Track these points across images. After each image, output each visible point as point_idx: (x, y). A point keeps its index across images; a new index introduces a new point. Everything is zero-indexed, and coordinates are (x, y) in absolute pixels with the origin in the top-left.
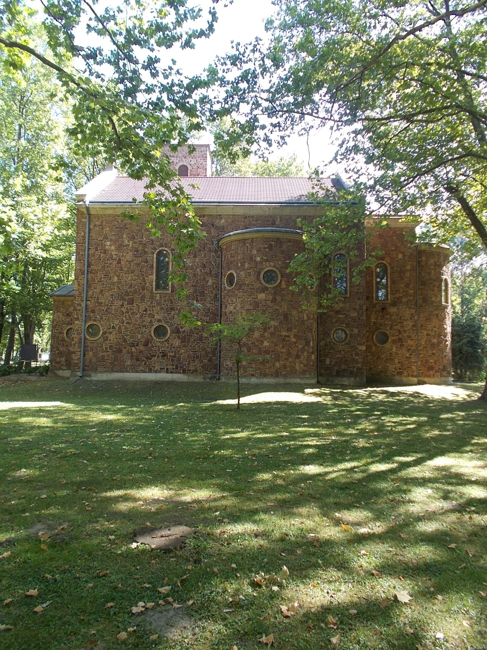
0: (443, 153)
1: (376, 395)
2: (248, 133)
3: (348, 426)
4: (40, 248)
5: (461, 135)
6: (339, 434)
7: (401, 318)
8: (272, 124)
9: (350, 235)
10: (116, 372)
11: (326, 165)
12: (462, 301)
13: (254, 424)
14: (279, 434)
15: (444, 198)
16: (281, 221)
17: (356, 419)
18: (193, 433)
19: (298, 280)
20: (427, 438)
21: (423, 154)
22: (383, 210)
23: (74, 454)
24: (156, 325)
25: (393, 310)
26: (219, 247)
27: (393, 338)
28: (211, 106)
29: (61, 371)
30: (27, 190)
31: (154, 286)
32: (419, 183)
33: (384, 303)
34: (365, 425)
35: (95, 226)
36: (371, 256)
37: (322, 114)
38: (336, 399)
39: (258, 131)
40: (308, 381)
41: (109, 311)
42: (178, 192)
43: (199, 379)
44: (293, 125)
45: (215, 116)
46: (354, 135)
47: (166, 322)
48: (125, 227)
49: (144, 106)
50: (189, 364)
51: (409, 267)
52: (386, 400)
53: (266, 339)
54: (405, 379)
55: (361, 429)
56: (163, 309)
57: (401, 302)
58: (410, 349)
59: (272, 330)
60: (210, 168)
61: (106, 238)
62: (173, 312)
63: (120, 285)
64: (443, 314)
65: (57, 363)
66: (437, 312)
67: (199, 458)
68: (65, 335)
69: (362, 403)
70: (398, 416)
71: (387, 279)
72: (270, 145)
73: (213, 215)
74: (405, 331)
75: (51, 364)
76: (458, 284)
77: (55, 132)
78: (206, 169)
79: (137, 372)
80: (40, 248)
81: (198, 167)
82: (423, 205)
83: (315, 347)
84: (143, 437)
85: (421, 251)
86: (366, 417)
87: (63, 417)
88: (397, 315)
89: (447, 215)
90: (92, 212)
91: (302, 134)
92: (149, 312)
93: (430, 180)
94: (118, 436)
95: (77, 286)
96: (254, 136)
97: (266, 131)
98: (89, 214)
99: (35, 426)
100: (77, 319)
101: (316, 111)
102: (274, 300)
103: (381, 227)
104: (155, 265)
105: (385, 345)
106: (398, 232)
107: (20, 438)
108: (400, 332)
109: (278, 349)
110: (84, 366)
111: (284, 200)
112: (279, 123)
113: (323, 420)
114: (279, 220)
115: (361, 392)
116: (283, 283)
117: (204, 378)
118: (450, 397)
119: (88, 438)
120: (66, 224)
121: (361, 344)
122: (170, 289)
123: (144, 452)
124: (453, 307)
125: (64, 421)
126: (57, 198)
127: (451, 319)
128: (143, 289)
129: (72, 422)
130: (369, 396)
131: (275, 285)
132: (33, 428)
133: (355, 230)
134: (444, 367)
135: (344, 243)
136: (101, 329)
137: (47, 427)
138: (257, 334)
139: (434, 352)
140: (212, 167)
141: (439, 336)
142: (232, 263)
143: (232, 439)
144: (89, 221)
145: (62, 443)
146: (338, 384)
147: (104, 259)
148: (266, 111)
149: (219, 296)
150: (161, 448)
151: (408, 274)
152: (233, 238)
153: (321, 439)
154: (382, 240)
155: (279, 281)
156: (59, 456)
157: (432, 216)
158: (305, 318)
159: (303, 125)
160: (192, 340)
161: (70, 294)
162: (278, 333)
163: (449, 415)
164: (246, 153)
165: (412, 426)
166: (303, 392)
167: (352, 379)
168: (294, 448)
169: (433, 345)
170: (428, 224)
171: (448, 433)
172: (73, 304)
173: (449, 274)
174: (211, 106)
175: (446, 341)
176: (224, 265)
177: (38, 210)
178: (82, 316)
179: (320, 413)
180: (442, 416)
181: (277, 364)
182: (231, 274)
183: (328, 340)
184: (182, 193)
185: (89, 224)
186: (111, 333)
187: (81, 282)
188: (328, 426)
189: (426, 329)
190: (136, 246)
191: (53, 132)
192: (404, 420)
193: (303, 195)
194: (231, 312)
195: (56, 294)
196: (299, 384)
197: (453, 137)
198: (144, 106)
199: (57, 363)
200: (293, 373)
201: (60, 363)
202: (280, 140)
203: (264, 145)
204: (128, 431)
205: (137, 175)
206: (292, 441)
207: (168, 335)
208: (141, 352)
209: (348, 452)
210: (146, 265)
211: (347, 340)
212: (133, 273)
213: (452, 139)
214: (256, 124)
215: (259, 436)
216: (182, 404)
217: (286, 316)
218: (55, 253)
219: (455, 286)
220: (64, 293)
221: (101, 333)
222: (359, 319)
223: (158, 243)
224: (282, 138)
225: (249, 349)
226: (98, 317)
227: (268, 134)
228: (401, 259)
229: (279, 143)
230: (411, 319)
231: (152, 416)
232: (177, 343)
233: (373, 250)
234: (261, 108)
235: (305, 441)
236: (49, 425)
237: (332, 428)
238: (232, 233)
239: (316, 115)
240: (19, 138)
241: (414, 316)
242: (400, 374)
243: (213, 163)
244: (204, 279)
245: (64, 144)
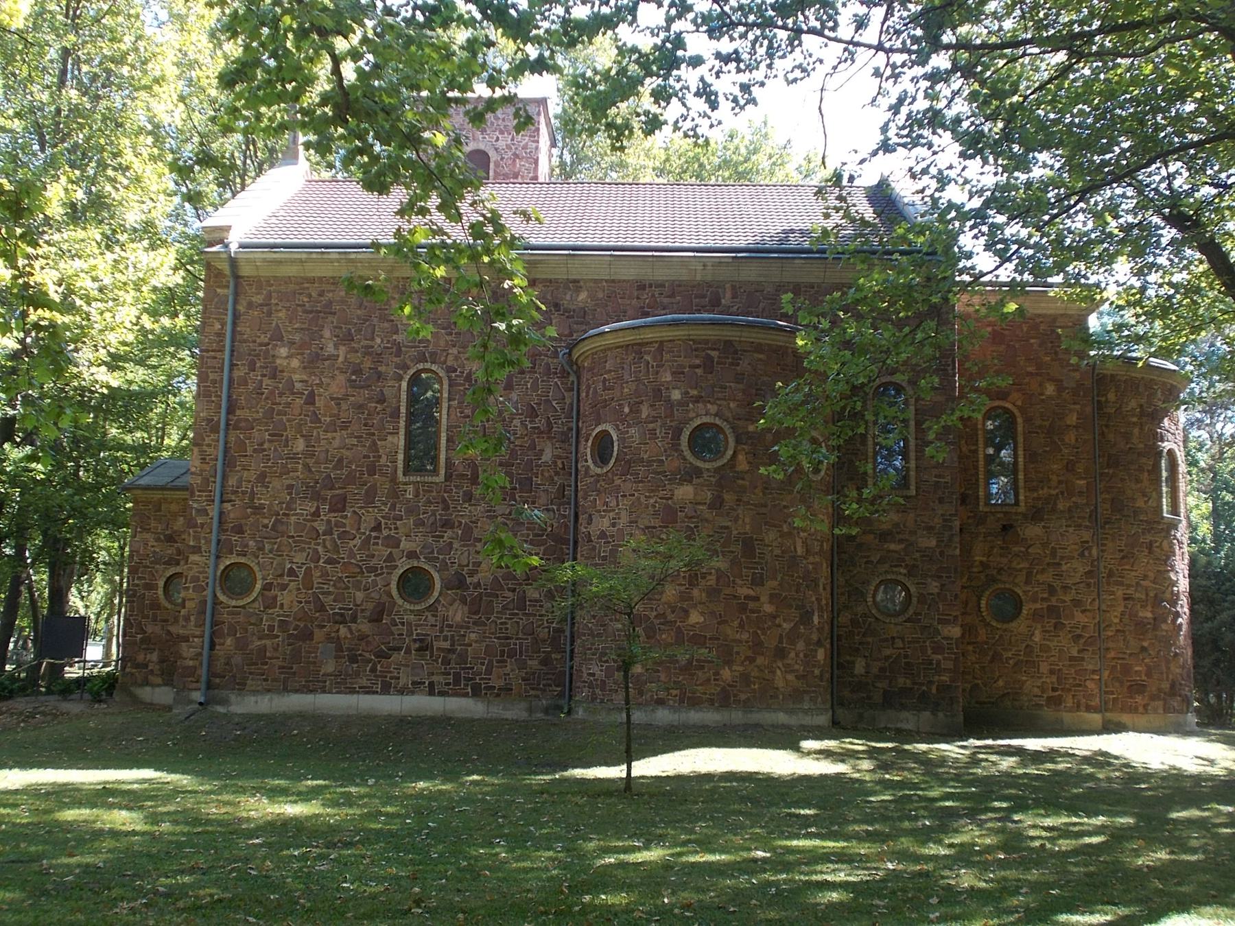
0: (1158, 128)
1: (993, 758)
2: (658, 76)
3: (926, 836)
4: (105, 363)
5: (1206, 86)
6: (903, 856)
7: (1053, 553)
8: (718, 56)
9: (919, 336)
10: (296, 691)
11: (862, 162)
12: (1215, 509)
13: (675, 828)
14: (745, 854)
15: (1164, 241)
16: (734, 296)
17: (945, 821)
18: (519, 852)
19: (783, 450)
20: (1139, 869)
21: (1108, 129)
22: (1006, 273)
23: (220, 901)
24: (403, 565)
25: (1032, 531)
26: (571, 363)
28: (567, 11)
29: (148, 689)
30: (75, 214)
31: (400, 464)
32: (1096, 204)
33: (1006, 513)
34: (969, 834)
35: (250, 305)
36: (977, 390)
37: (846, 30)
38: (884, 767)
39: (684, 71)
40: (808, 720)
41: (281, 528)
42: (489, 229)
43: (515, 712)
44: (770, 56)
45: (576, 34)
46: (928, 84)
47: (429, 559)
48: (328, 310)
49: (403, 13)
50: (489, 671)
51: (1072, 419)
52: (1020, 771)
53: (695, 606)
54: (1067, 717)
55: (962, 845)
56: (423, 524)
57: (1054, 510)
58: (1080, 636)
59: (712, 581)
60: (547, 159)
61: (278, 337)
62: (449, 533)
63: (311, 462)
64: (1165, 544)
65: (137, 666)
66: (1149, 538)
67: (546, 913)
68: (160, 592)
69: (957, 778)
70: (1058, 814)
71: (1015, 450)
72: (714, 106)
73: (556, 281)
74: (1066, 588)
75: (123, 668)
76: (1202, 464)
77: (155, 69)
78: (536, 162)
79: (352, 691)
80: (105, 363)
81: (516, 156)
82: (1107, 260)
83: (827, 628)
84: (388, 860)
85: (1105, 376)
86: (972, 814)
87: (172, 808)
88: (1045, 545)
89: (1170, 284)
90: (245, 271)
91: (795, 80)
92: (385, 533)
93: (1124, 196)
94: (321, 857)
95: (197, 463)
96: (671, 81)
97: (702, 70)
98: (237, 277)
99: (101, 831)
100: (197, 550)
101: (831, 24)
102: (717, 504)
103: (1005, 316)
104: (403, 410)
105: (1014, 624)
106: (1042, 327)
107: (73, 860)
109: (729, 631)
110: (212, 674)
111: (742, 243)
112: (736, 52)
113: (855, 821)
114: (728, 295)
115: (951, 750)
116: (741, 457)
117: (530, 710)
118: (1191, 767)
119: (247, 860)
120: (169, 301)
121: (946, 622)
122: (442, 472)
123: (399, 896)
124: (1193, 528)
125: (174, 818)
126: (148, 233)
127: (1187, 556)
128: (372, 472)
129: (197, 821)
130: (974, 761)
131: (719, 463)
132: (99, 834)
133: (933, 324)
134: (1173, 686)
135: (904, 356)
136: (259, 576)
137: (134, 833)
138: (670, 592)
139: (1145, 644)
140: (551, 156)
141: (1157, 600)
142: (605, 404)
143: (623, 865)
144: (236, 294)
145: (182, 872)
146: (888, 729)
147: (272, 392)
148: (704, 22)
149: (569, 492)
150: (442, 888)
151: (1071, 437)
152: (610, 341)
153: (857, 868)
154: (1002, 348)
155: (730, 453)
156: (181, 904)
157: (1132, 287)
158: (800, 551)
159: (797, 56)
160: (498, 607)
161: (178, 483)
162: (728, 591)
163: (1194, 813)
164: (653, 124)
165: (1095, 840)
166: (797, 749)
167: (927, 714)
168: (790, 891)
169: (1141, 627)
170: (1121, 308)
171: (1194, 858)
172: (185, 510)
173: (1180, 438)
174: (567, 11)
175: (1177, 615)
176: (586, 408)
177: (103, 264)
178: (208, 542)
179: (846, 803)
180: (1174, 815)
181: (726, 674)
182: (605, 435)
183: (860, 609)
184: (500, 229)
185: (236, 302)
186: (284, 587)
187: (209, 450)
188: (870, 837)
189: (1121, 584)
190: (356, 358)
191: (150, 66)
192: (1075, 824)
193: (793, 232)
194: (603, 535)
195: (142, 482)
196: (784, 726)
197: (1184, 89)
198: (403, 13)
199: (137, 666)
201: (146, 666)
202: (739, 94)
203: (699, 105)
204: (348, 845)
205: (376, 184)
206: (781, 872)
207: (436, 594)
208: (363, 638)
209: (934, 901)
210: (379, 407)
211: (911, 611)
212: (346, 428)
213: (1182, 96)
214: (680, 53)
215: (692, 859)
216: (475, 777)
217: (749, 545)
218: (137, 375)
219: (1195, 470)
220: (162, 481)
221: (258, 586)
222: (942, 553)
223: (413, 352)
224: (745, 88)
225: (651, 633)
226: (251, 543)
227: (710, 79)
228: (1050, 398)
229: (735, 100)
230: (1082, 555)
231: (403, 806)
232: (458, 614)
233: (981, 375)
234: (691, 16)
235: (816, 873)
236: (138, 828)
237: (884, 842)
238: (606, 328)
239: (832, 34)
240: (62, 83)
241: (1089, 549)
242: (1055, 702)
243: (553, 144)
244: (533, 446)
245: (175, 97)
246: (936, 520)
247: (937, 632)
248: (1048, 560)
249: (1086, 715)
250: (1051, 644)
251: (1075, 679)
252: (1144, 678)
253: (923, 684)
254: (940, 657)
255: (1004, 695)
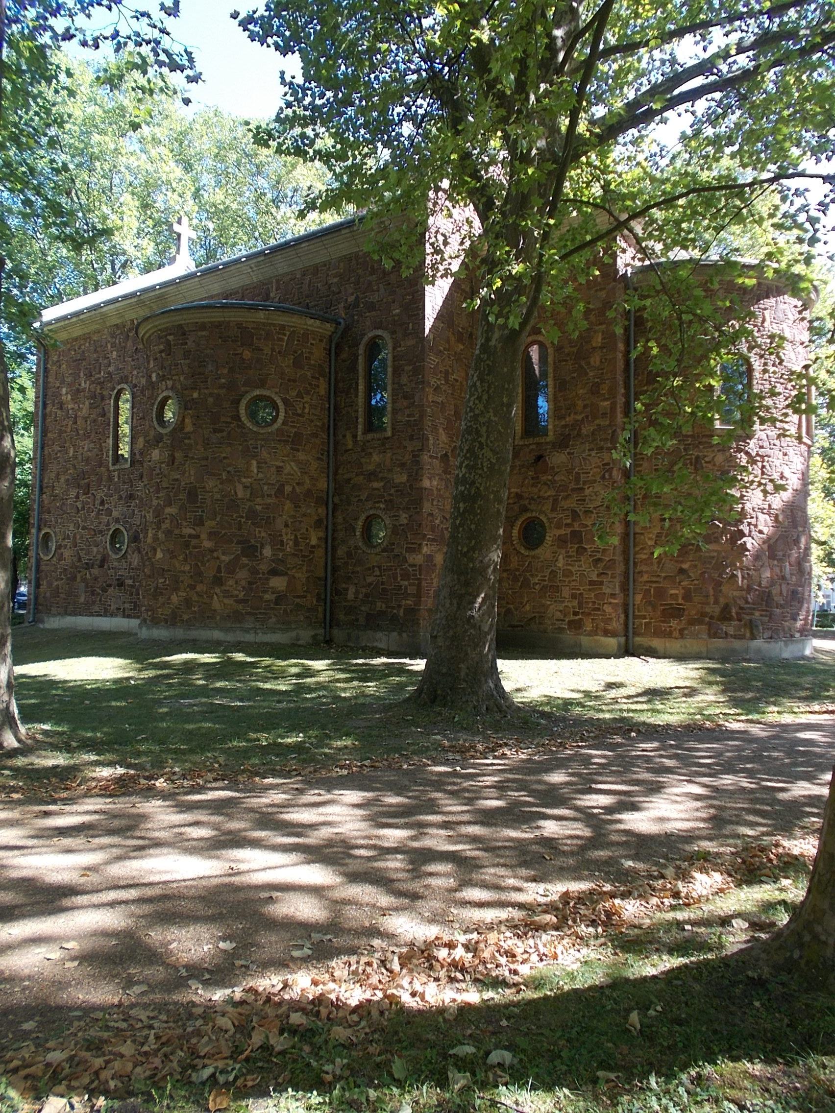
27: (558, 532)
54: (585, 641)
57: (579, 435)
58: (599, 560)
74: (587, 512)
105: (537, 552)
108: (575, 515)
139: (685, 566)
162: (177, 532)
181: (174, 598)
200: (206, 617)
230: (603, 477)
242: (576, 626)
246: (407, 457)
247: (405, 560)
248: (572, 486)
249: (603, 639)
250: (573, 569)
251: (594, 603)
252: (680, 601)
253: (393, 608)
254: (406, 583)
255: (531, 619)
